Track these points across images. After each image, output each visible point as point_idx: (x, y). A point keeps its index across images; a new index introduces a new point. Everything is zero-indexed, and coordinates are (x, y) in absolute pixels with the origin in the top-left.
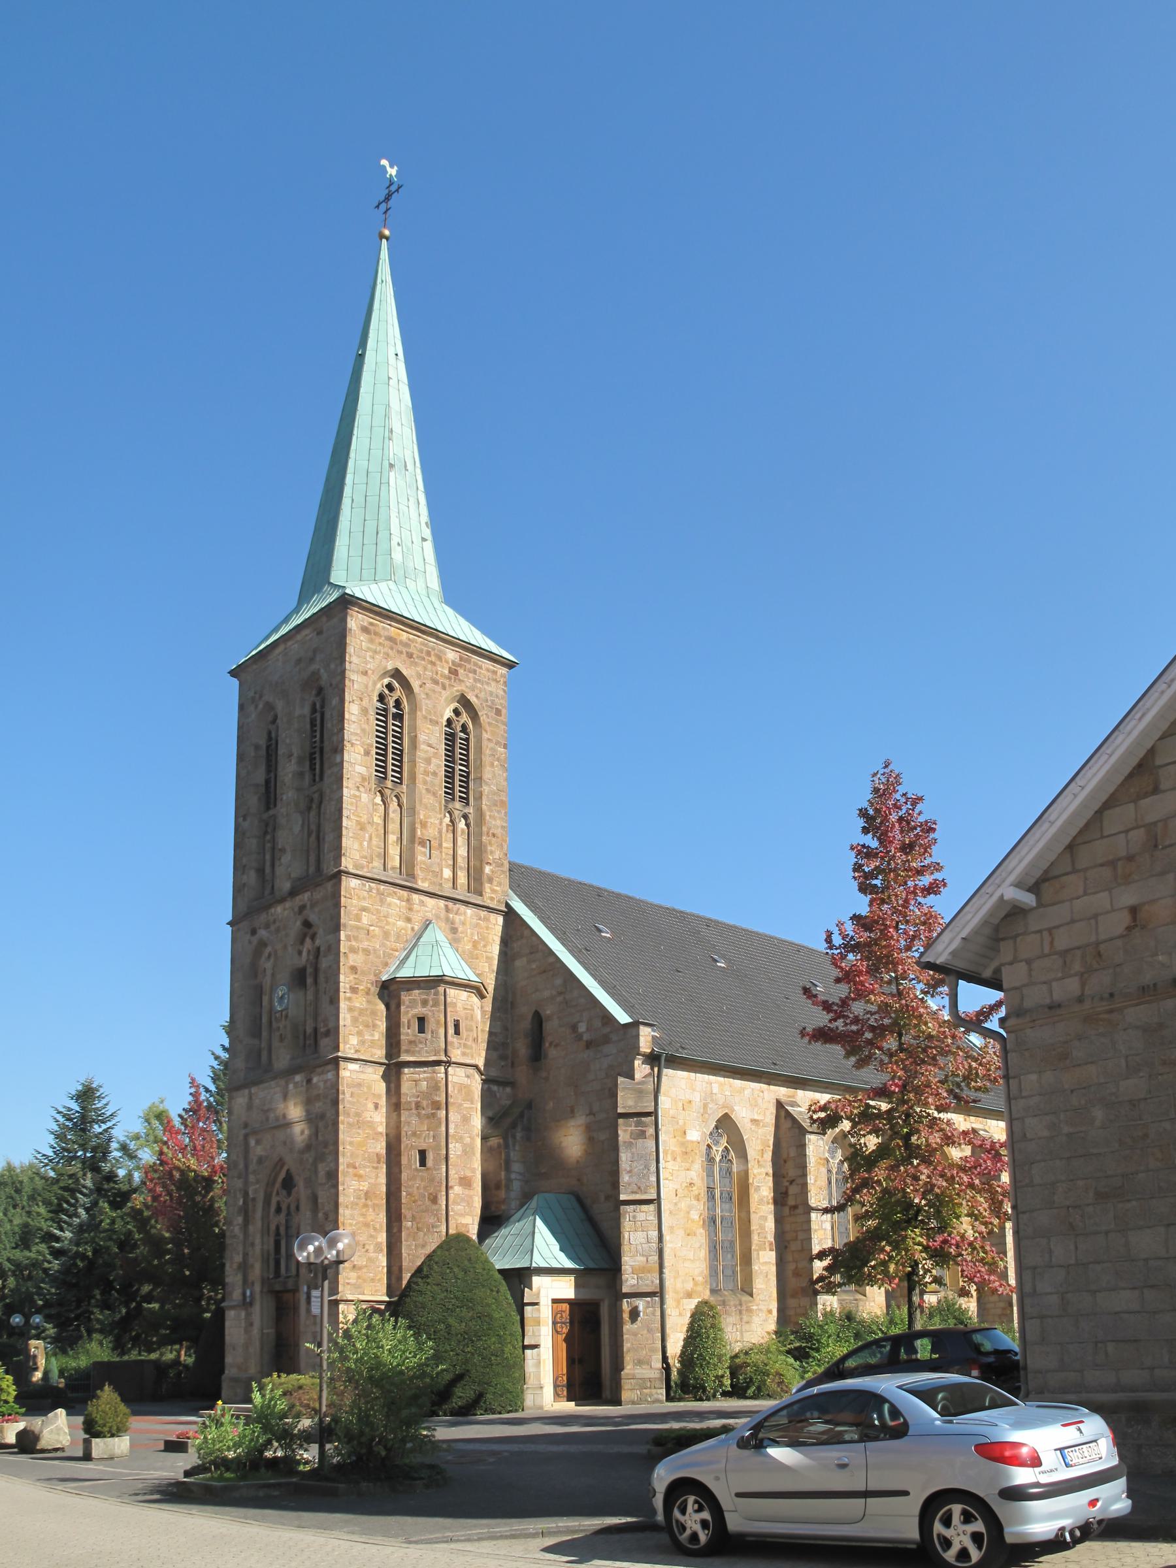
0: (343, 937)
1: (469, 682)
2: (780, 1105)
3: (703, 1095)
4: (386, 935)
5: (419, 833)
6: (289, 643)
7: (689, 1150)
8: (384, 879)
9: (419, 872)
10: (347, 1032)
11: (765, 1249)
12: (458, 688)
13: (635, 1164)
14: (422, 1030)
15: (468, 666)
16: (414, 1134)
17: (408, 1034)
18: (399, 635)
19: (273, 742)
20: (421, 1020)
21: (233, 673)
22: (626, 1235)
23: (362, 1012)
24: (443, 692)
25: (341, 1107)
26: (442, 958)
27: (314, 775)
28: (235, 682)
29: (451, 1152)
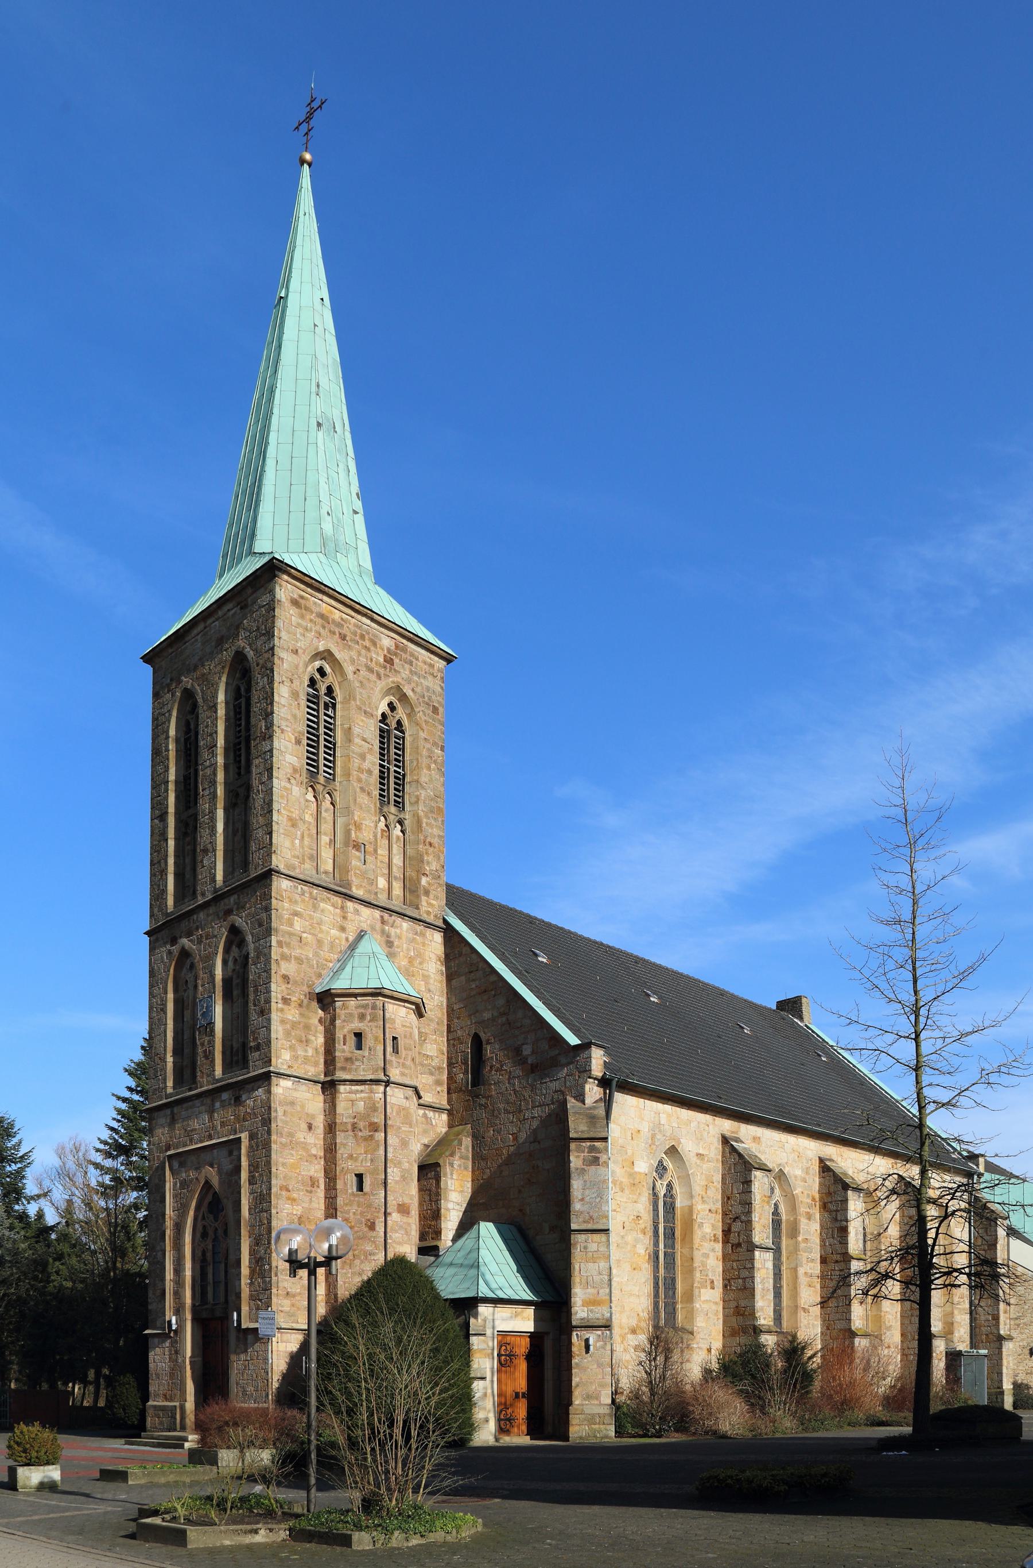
0: (274, 943)
1: (405, 673)
2: (725, 1140)
3: (651, 1125)
4: (320, 943)
5: (353, 835)
6: (209, 621)
7: (637, 1181)
8: (317, 882)
9: (354, 879)
10: (279, 1046)
11: (706, 1287)
12: (392, 679)
13: (587, 1192)
14: (359, 1047)
15: (404, 656)
16: (351, 1157)
17: (344, 1051)
18: (331, 613)
19: (192, 734)
20: (358, 1035)
21: (147, 659)
22: (577, 1267)
23: (294, 1025)
24: (378, 682)
25: (273, 1125)
26: (380, 970)
27: (239, 768)
28: (148, 669)
29: (389, 1177)
